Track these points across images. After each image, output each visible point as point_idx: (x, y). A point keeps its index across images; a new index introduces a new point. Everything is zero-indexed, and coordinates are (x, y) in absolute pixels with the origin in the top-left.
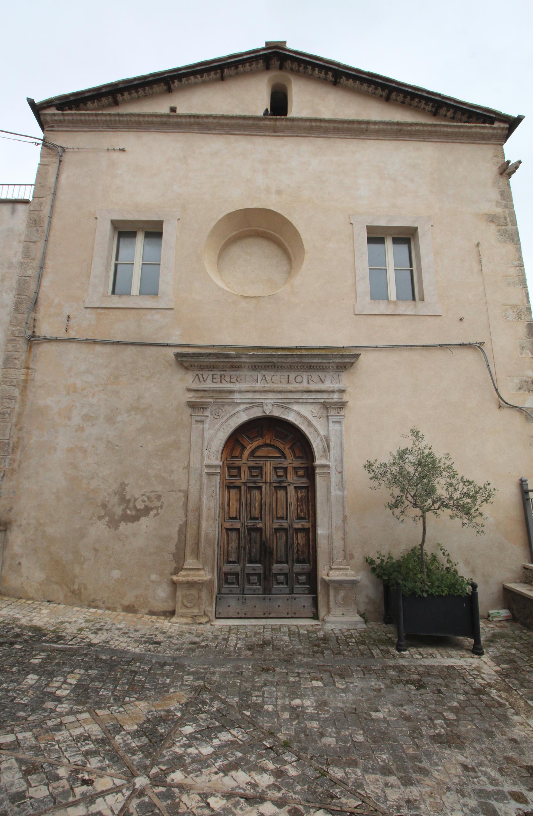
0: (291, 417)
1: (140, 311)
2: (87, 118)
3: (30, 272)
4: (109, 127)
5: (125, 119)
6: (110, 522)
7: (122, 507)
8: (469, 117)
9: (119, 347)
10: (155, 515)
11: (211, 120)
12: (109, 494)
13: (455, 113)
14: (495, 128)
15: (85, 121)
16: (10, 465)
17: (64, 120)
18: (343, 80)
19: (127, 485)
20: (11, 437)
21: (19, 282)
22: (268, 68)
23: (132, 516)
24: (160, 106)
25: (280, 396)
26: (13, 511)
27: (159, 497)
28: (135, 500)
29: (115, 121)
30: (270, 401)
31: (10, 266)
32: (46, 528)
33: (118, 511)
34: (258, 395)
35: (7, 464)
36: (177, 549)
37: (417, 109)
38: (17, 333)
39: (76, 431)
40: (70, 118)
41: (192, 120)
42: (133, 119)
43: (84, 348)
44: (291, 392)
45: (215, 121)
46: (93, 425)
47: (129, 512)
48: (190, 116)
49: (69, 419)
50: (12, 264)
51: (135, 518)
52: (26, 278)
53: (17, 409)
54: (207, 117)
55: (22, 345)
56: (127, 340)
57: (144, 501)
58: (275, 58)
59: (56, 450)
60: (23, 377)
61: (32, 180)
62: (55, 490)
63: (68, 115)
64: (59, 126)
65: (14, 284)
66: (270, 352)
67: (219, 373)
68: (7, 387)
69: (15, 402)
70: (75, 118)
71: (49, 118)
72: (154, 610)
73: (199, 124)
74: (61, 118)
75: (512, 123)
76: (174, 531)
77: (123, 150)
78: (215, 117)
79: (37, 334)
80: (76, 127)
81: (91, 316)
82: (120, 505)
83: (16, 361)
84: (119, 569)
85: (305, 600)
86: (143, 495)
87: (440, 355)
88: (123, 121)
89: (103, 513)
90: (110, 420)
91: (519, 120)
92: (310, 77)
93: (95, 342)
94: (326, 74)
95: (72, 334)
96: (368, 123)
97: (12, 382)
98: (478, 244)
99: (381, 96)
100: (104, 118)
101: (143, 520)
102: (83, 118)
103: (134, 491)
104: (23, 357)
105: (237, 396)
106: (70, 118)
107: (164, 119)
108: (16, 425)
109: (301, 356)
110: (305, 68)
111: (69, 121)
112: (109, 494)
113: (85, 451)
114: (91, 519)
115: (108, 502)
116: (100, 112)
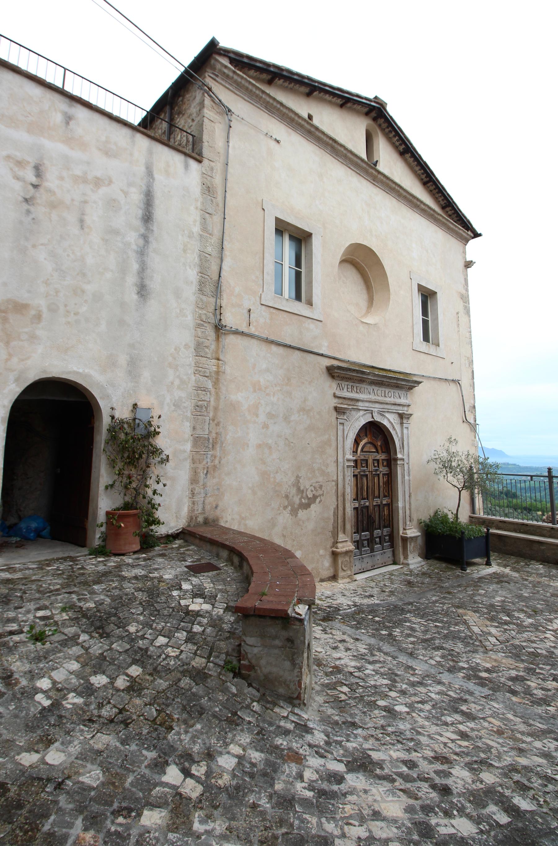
0: (385, 423)
1: (301, 317)
2: (254, 90)
3: (209, 249)
4: (266, 108)
5: (285, 110)
7: (299, 497)
8: (458, 220)
9: (290, 351)
10: (320, 502)
11: (342, 149)
12: (289, 486)
13: (453, 214)
14: (468, 234)
15: (251, 91)
16: (212, 461)
17: (233, 78)
20: (210, 432)
22: (367, 114)
24: (302, 107)
26: (219, 508)
27: (321, 487)
29: (275, 107)
30: (376, 410)
31: (191, 236)
32: (247, 522)
33: (297, 500)
34: (371, 405)
35: (209, 460)
36: (333, 528)
37: (436, 199)
38: (204, 318)
39: (263, 428)
40: (239, 80)
41: (331, 142)
43: (264, 347)
44: (387, 404)
45: (345, 152)
46: (275, 423)
47: (303, 501)
48: (331, 138)
49: (257, 416)
50: (193, 233)
51: (307, 506)
52: (207, 255)
53: (212, 403)
54: (341, 145)
55: (210, 332)
56: (293, 344)
58: (376, 113)
59: (248, 446)
60: (214, 369)
61: (149, 108)
62: (250, 485)
63: (238, 75)
64: (223, 80)
65: (197, 260)
66: (384, 374)
67: (351, 384)
68: (201, 378)
69: (210, 394)
70: (243, 82)
71: (218, 66)
72: (323, 578)
73: (332, 147)
74: (231, 74)
75: (477, 235)
77: (278, 142)
78: (346, 149)
82: (297, 495)
84: (300, 550)
85: (389, 552)
86: (311, 485)
88: (282, 111)
89: (286, 504)
90: (286, 419)
91: (480, 235)
92: (389, 139)
93: (272, 342)
94: (401, 145)
95: (252, 330)
96: (422, 202)
97: (205, 372)
99: (422, 179)
100: (268, 99)
101: (313, 506)
102: (250, 87)
103: (305, 484)
105: (360, 404)
106: (239, 80)
107: (313, 129)
109: (398, 379)
110: (390, 132)
111: (236, 82)
112: (289, 486)
114: (279, 509)
115: (289, 493)
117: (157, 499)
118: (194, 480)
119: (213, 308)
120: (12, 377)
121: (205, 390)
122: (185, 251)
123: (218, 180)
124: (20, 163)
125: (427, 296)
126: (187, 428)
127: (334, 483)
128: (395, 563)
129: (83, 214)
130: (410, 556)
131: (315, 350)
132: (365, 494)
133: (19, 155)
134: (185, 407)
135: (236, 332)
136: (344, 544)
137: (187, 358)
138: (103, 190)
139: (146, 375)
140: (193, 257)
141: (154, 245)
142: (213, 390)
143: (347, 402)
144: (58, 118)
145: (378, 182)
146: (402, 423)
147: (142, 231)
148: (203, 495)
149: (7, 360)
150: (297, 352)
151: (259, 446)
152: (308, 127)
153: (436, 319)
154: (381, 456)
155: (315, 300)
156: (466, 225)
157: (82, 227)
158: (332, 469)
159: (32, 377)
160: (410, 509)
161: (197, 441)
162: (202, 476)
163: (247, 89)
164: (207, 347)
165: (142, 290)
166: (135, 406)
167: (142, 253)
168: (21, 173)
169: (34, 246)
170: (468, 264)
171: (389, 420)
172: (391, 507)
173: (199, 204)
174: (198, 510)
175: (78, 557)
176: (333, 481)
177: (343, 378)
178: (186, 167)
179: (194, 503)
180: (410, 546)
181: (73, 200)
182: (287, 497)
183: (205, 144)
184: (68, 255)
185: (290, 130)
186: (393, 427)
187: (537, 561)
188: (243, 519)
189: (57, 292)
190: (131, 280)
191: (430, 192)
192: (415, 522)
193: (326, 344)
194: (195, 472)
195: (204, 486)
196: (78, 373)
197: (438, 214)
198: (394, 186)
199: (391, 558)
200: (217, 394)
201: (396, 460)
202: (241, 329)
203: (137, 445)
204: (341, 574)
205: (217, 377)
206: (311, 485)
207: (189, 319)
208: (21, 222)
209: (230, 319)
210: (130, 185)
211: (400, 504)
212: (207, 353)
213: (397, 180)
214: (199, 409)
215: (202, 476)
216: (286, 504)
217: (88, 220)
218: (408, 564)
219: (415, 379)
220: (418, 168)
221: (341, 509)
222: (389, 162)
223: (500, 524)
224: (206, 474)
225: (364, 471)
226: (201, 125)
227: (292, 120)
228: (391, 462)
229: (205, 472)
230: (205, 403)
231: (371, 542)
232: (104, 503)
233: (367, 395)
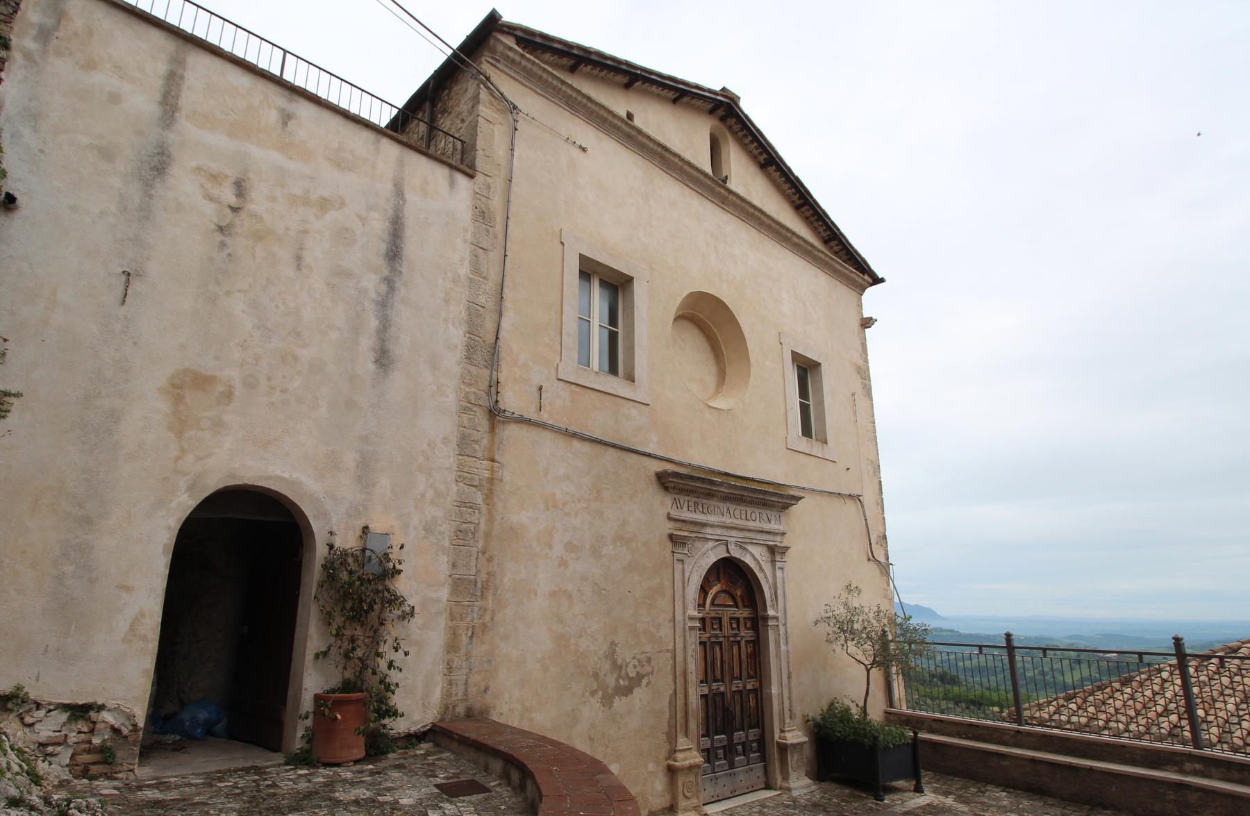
0: (748, 560)
3: (482, 300)
4: (567, 104)
6: (604, 697)
7: (615, 676)
10: (648, 685)
15: (546, 81)
18: (771, 169)
19: (616, 645)
20: (478, 571)
22: (711, 112)
23: (626, 687)
24: (618, 103)
25: (741, 534)
26: (490, 692)
27: (649, 660)
28: (627, 664)
33: (611, 681)
34: (725, 532)
36: (669, 726)
37: (815, 230)
39: (559, 566)
40: (529, 66)
41: (659, 150)
42: (602, 112)
43: (561, 442)
44: (750, 530)
45: (680, 163)
47: (622, 682)
48: (660, 145)
49: (551, 547)
51: (627, 691)
53: (483, 527)
54: (675, 155)
55: (482, 420)
56: (605, 439)
57: (635, 667)
58: (724, 111)
60: (487, 474)
63: (528, 60)
65: (464, 315)
68: (466, 488)
70: (535, 69)
71: (500, 48)
74: (518, 59)
75: (877, 280)
76: (666, 702)
77: (584, 150)
79: (501, 406)
80: (530, 81)
81: (564, 391)
87: (837, 503)
89: (595, 687)
90: (595, 552)
91: (882, 280)
92: (744, 146)
93: (574, 435)
94: (761, 154)
95: (545, 417)
97: (472, 479)
98: (853, 394)
100: (570, 92)
101: (636, 690)
103: (624, 655)
104: (485, 442)
105: (708, 530)
106: (529, 66)
107: (633, 133)
109: (765, 493)
110: (746, 136)
111: (524, 69)
116: (550, 69)
117: (394, 676)
119: (487, 384)
120: (183, 484)
121: (473, 506)
122: (446, 301)
123: (497, 203)
124: (215, 178)
125: (806, 370)
126: (442, 565)
127: (669, 655)
128: (768, 787)
129: (301, 249)
130: (793, 776)
132: (718, 672)
133: (214, 166)
134: (441, 533)
135: (521, 420)
136: (687, 754)
137: (447, 457)
138: (331, 216)
139: (384, 482)
140: (458, 310)
141: (401, 292)
142: (484, 507)
144: (273, 117)
146: (773, 561)
147: (386, 272)
148: (465, 671)
149: (177, 459)
150: (611, 450)
151: (553, 594)
153: (820, 403)
154: (743, 613)
155: (638, 373)
157: (299, 267)
158: (666, 632)
159: (214, 483)
160: (790, 698)
161: (458, 584)
162: (465, 639)
163: (541, 78)
165: (383, 358)
166: (366, 529)
167: (384, 304)
168: (215, 192)
169: (228, 293)
170: (867, 323)
171: (753, 556)
173: (469, 236)
175: (267, 767)
178: (452, 184)
179: (450, 683)
180: (793, 759)
181: (287, 229)
183: (480, 153)
184: (277, 307)
185: (601, 135)
187: (998, 785)
189: (258, 359)
190: (367, 342)
192: (799, 720)
193: (655, 439)
194: (454, 634)
195: (468, 655)
196: (282, 478)
198: (752, 210)
199: (762, 779)
200: (490, 513)
201: (766, 618)
202: (527, 416)
203: (366, 590)
204: (683, 803)
205: (490, 487)
207: (451, 400)
208: (211, 259)
209: (512, 400)
210: (370, 208)
211: (774, 690)
212: (475, 451)
213: (757, 203)
214: (462, 535)
215: (465, 639)
216: (595, 687)
217: (308, 257)
218: (789, 790)
219: (791, 492)
221: (680, 696)
222: (743, 176)
223: (934, 725)
224: (471, 637)
225: (716, 636)
226: (474, 128)
227: (604, 120)
228: (758, 622)
230: (472, 527)
231: (729, 751)
232: (312, 681)
233: (717, 516)
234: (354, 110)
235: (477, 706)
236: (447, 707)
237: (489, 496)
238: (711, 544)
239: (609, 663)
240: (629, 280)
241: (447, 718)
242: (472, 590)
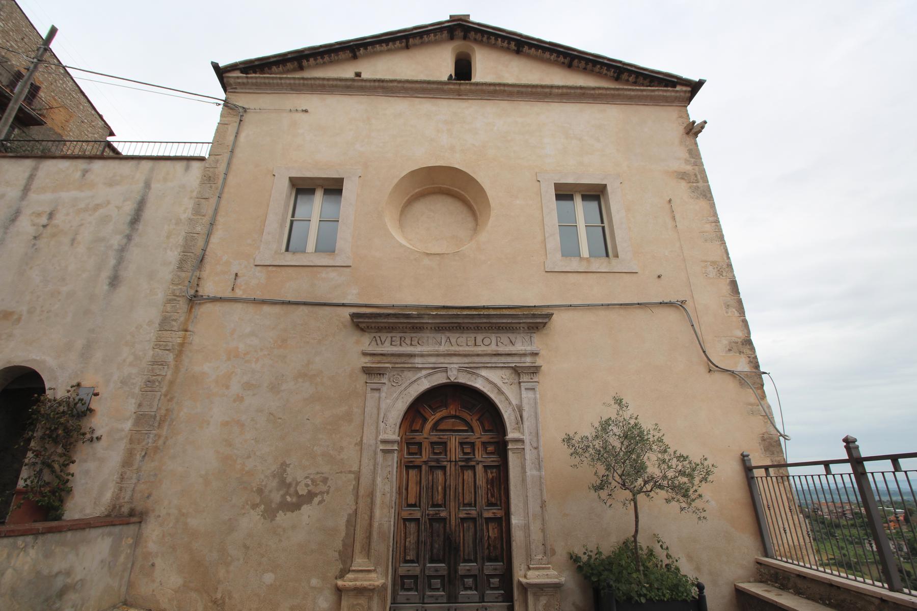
0: (479, 384)
1: (315, 269)
4: (292, 89)
5: (309, 82)
6: (265, 511)
7: (282, 492)
10: (320, 503)
11: (396, 84)
12: (266, 477)
14: (677, 91)
16: (155, 442)
20: (159, 409)
21: (186, 239)
26: (152, 498)
27: (325, 480)
28: (297, 483)
29: (299, 84)
30: (456, 366)
33: (276, 497)
35: (150, 441)
36: (344, 545)
37: (599, 75)
39: (235, 401)
40: (254, 81)
41: (377, 84)
42: (317, 82)
43: (251, 309)
44: (478, 355)
45: (400, 85)
46: (254, 395)
47: (289, 499)
48: (375, 81)
49: (228, 387)
51: (296, 507)
53: (169, 377)
54: (392, 81)
55: (183, 305)
58: (459, 30)
60: (179, 341)
63: (252, 78)
66: (455, 312)
68: (160, 352)
70: (259, 81)
73: (383, 88)
74: (245, 81)
75: (695, 87)
76: (342, 522)
77: (306, 111)
83: (174, 323)
89: (258, 500)
91: (700, 83)
93: (264, 302)
94: (509, 43)
95: (239, 293)
97: (166, 345)
98: (670, 201)
99: (563, 63)
100: (288, 82)
101: (305, 508)
102: (267, 81)
103: (297, 473)
105: (418, 360)
106: (254, 81)
108: (166, 395)
110: (488, 38)
111: (253, 84)
113: (242, 425)
115: (265, 486)
118: (127, 462)
121: (163, 364)
122: (168, 237)
126: (131, 406)
131: (335, 301)
138: (101, 211)
141: (136, 239)
143: (389, 359)
145: (466, 95)
148: (134, 481)
151: (226, 424)
152: (360, 84)
156: (667, 81)
157: (72, 244)
161: (141, 419)
162: (138, 457)
163: (265, 84)
164: (175, 320)
165: (115, 281)
169: (31, 268)
172: (504, 522)
174: (124, 498)
176: (350, 472)
177: (379, 329)
179: (121, 489)
182: (260, 491)
186: (499, 390)
188: (183, 515)
190: (106, 274)
191: (585, 71)
194: (130, 453)
195: (139, 470)
196: (35, 360)
197: (594, 89)
198: (492, 88)
205: (180, 350)
206: (307, 478)
212: (173, 326)
213: (511, 81)
214: (150, 385)
215: (138, 457)
216: (258, 500)
219: (545, 312)
220: (398, 43)
222: (488, 67)
223: (799, 582)
224: (144, 456)
227: (324, 86)
228: (501, 447)
229: (143, 454)
230: (159, 378)
233: (428, 346)
234: (155, 154)
235: (139, 508)
236: (114, 507)
237: (179, 355)
238: (424, 372)
239: (276, 480)
240: (604, 187)
241: (113, 514)
242: (152, 424)
